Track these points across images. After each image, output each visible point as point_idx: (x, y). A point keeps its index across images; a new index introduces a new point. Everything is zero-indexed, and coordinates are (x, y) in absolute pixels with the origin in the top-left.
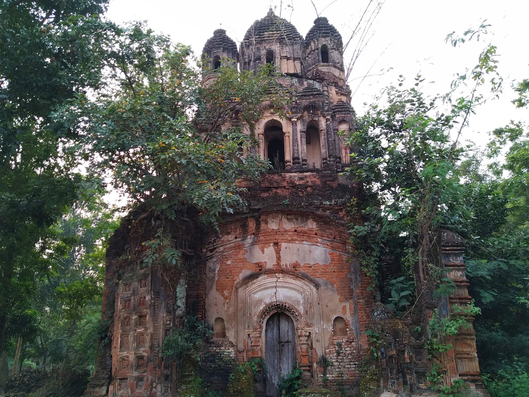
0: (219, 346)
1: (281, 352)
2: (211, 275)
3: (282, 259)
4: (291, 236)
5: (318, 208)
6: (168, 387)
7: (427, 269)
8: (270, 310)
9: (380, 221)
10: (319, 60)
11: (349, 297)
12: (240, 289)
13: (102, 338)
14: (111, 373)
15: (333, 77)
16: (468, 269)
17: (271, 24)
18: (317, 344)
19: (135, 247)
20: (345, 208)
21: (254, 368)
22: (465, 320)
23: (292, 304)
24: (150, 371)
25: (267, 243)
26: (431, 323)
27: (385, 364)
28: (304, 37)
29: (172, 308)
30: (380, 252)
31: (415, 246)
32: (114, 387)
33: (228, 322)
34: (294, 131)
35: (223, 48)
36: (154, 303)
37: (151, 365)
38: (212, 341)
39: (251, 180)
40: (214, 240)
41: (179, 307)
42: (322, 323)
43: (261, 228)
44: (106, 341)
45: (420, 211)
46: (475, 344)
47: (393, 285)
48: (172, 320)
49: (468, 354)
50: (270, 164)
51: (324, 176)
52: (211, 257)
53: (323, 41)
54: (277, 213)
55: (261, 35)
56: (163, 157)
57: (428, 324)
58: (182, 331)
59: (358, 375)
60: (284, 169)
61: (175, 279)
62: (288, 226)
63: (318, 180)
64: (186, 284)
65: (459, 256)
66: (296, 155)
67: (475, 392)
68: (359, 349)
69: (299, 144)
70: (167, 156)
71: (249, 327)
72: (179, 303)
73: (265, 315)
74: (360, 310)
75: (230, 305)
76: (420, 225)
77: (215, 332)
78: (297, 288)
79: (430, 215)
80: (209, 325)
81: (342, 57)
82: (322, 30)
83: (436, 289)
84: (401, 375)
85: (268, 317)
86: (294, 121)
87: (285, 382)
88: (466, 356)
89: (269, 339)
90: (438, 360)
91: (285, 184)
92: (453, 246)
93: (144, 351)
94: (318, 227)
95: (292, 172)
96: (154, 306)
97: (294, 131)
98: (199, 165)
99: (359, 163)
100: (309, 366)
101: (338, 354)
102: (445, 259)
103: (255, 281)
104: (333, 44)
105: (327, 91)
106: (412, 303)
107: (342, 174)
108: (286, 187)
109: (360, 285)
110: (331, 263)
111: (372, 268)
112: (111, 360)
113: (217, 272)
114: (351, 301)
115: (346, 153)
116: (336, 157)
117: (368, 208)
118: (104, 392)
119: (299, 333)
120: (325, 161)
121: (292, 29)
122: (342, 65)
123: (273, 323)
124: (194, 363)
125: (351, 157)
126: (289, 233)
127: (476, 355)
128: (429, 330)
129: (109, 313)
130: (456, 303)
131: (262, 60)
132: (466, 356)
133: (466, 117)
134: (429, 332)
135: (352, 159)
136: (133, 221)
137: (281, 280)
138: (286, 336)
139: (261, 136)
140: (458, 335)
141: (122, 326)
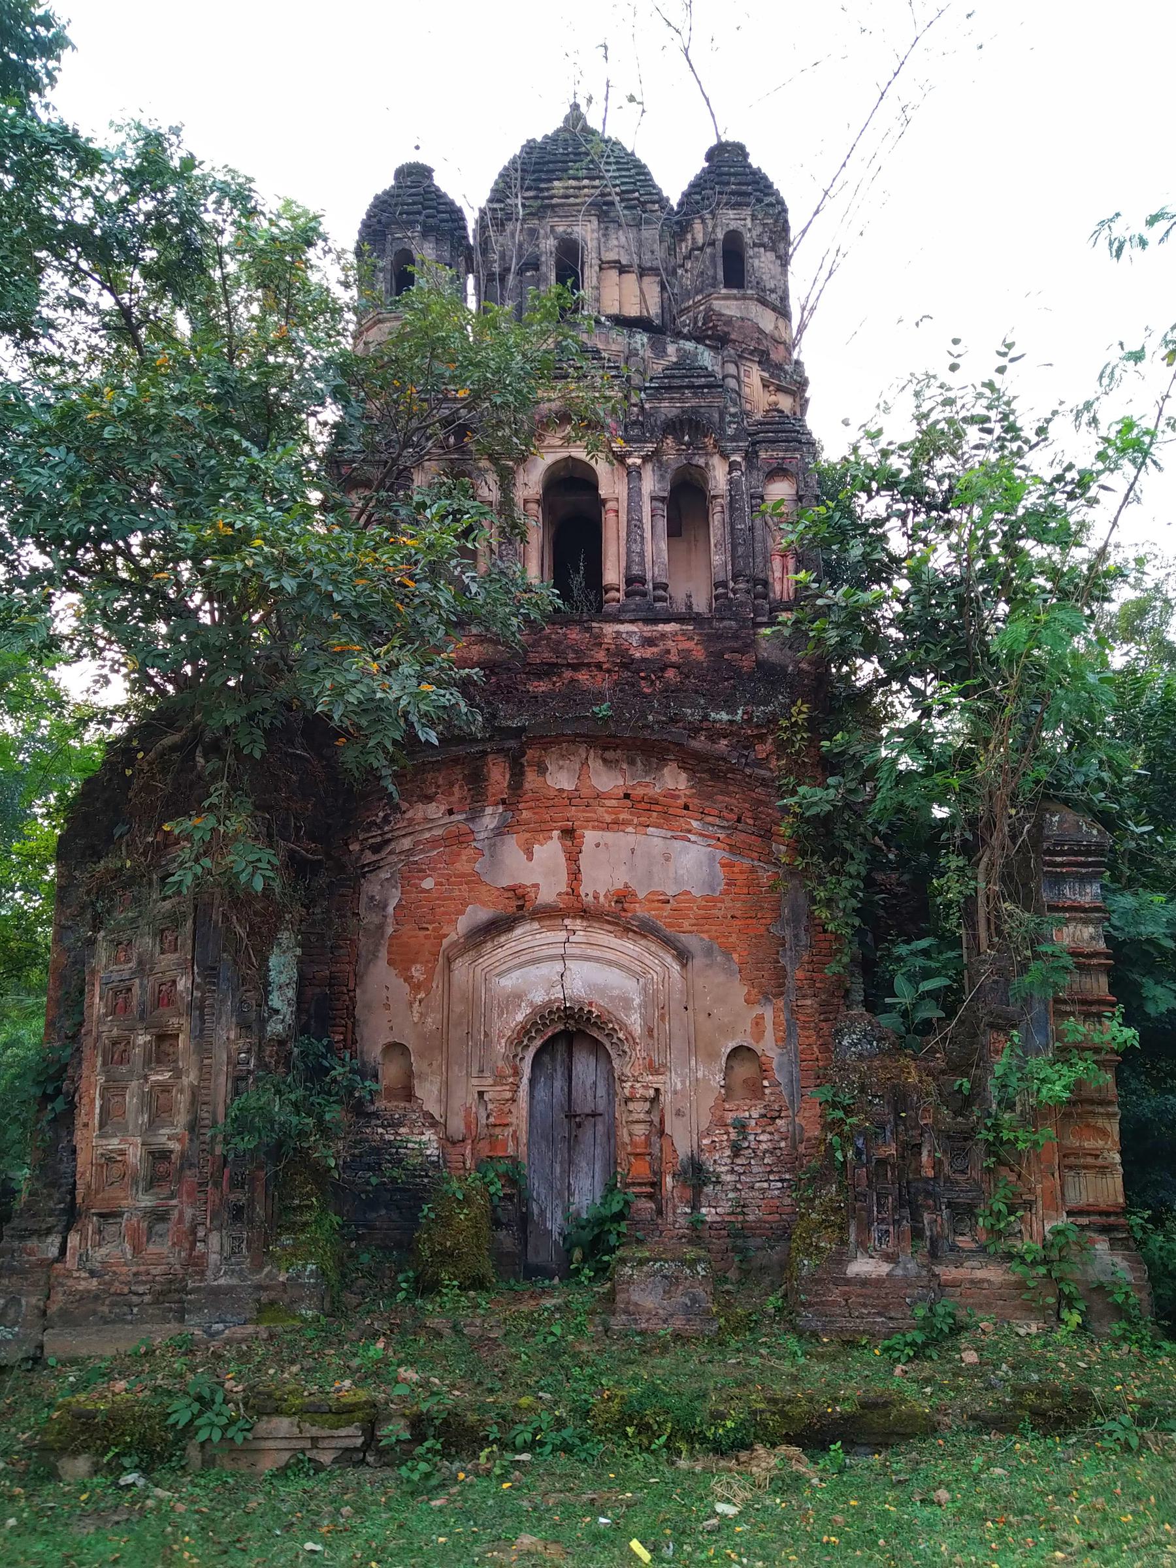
0: (395, 1125)
1: (572, 1142)
2: (370, 919)
3: (584, 877)
4: (614, 810)
5: (695, 731)
6: (241, 1241)
7: (998, 917)
8: (544, 1024)
10: (715, 278)
12: (458, 963)
13: (47, 1098)
14: (74, 1198)
17: (576, 154)
18: (678, 1122)
19: (147, 834)
20: (772, 732)
21: (492, 1189)
22: (1095, 1062)
23: (610, 1007)
24: (189, 1195)
25: (541, 830)
26: (999, 1070)
27: (864, 1182)
28: (674, 202)
29: (253, 1015)
31: (968, 850)
32: (84, 1238)
33: (421, 1056)
34: (634, 494)
35: (424, 225)
36: (203, 999)
38: (372, 1108)
40: (386, 817)
41: (277, 1012)
42: (693, 1062)
43: (527, 786)
44: (59, 1105)
45: (987, 751)
47: (900, 959)
49: (1097, 1156)
51: (718, 637)
52: (376, 867)
53: (730, 219)
54: (574, 742)
57: (992, 1072)
60: (599, 609)
61: (264, 930)
62: (606, 781)
65: (1091, 883)
66: (636, 570)
67: (1108, 1259)
69: (648, 535)
70: (239, 566)
72: (276, 1001)
73: (531, 1039)
74: (803, 1028)
78: (625, 960)
80: (364, 1064)
82: (728, 183)
84: (906, 1212)
85: (538, 1043)
88: (1090, 1160)
89: (540, 1107)
91: (601, 656)
92: (1076, 854)
93: (172, 1137)
94: (692, 787)
95: (622, 622)
96: (201, 1008)
97: (634, 494)
98: (335, 595)
99: (820, 602)
100: (653, 1185)
101: (736, 1151)
102: (1051, 889)
103: (503, 939)
104: (759, 229)
106: (951, 1013)
107: (768, 631)
109: (806, 958)
110: (726, 892)
112: (75, 1160)
113: (390, 910)
114: (780, 1003)
115: (784, 568)
116: (756, 581)
117: (839, 736)
118: (54, 1252)
120: (721, 590)
122: (784, 298)
123: (553, 1059)
124: (319, 1174)
126: (608, 803)
127: (1117, 1158)
131: (544, 269)
132: (1090, 1160)
134: (993, 1092)
136: (140, 755)
138: (590, 1098)
139: (533, 506)
141: (104, 1064)
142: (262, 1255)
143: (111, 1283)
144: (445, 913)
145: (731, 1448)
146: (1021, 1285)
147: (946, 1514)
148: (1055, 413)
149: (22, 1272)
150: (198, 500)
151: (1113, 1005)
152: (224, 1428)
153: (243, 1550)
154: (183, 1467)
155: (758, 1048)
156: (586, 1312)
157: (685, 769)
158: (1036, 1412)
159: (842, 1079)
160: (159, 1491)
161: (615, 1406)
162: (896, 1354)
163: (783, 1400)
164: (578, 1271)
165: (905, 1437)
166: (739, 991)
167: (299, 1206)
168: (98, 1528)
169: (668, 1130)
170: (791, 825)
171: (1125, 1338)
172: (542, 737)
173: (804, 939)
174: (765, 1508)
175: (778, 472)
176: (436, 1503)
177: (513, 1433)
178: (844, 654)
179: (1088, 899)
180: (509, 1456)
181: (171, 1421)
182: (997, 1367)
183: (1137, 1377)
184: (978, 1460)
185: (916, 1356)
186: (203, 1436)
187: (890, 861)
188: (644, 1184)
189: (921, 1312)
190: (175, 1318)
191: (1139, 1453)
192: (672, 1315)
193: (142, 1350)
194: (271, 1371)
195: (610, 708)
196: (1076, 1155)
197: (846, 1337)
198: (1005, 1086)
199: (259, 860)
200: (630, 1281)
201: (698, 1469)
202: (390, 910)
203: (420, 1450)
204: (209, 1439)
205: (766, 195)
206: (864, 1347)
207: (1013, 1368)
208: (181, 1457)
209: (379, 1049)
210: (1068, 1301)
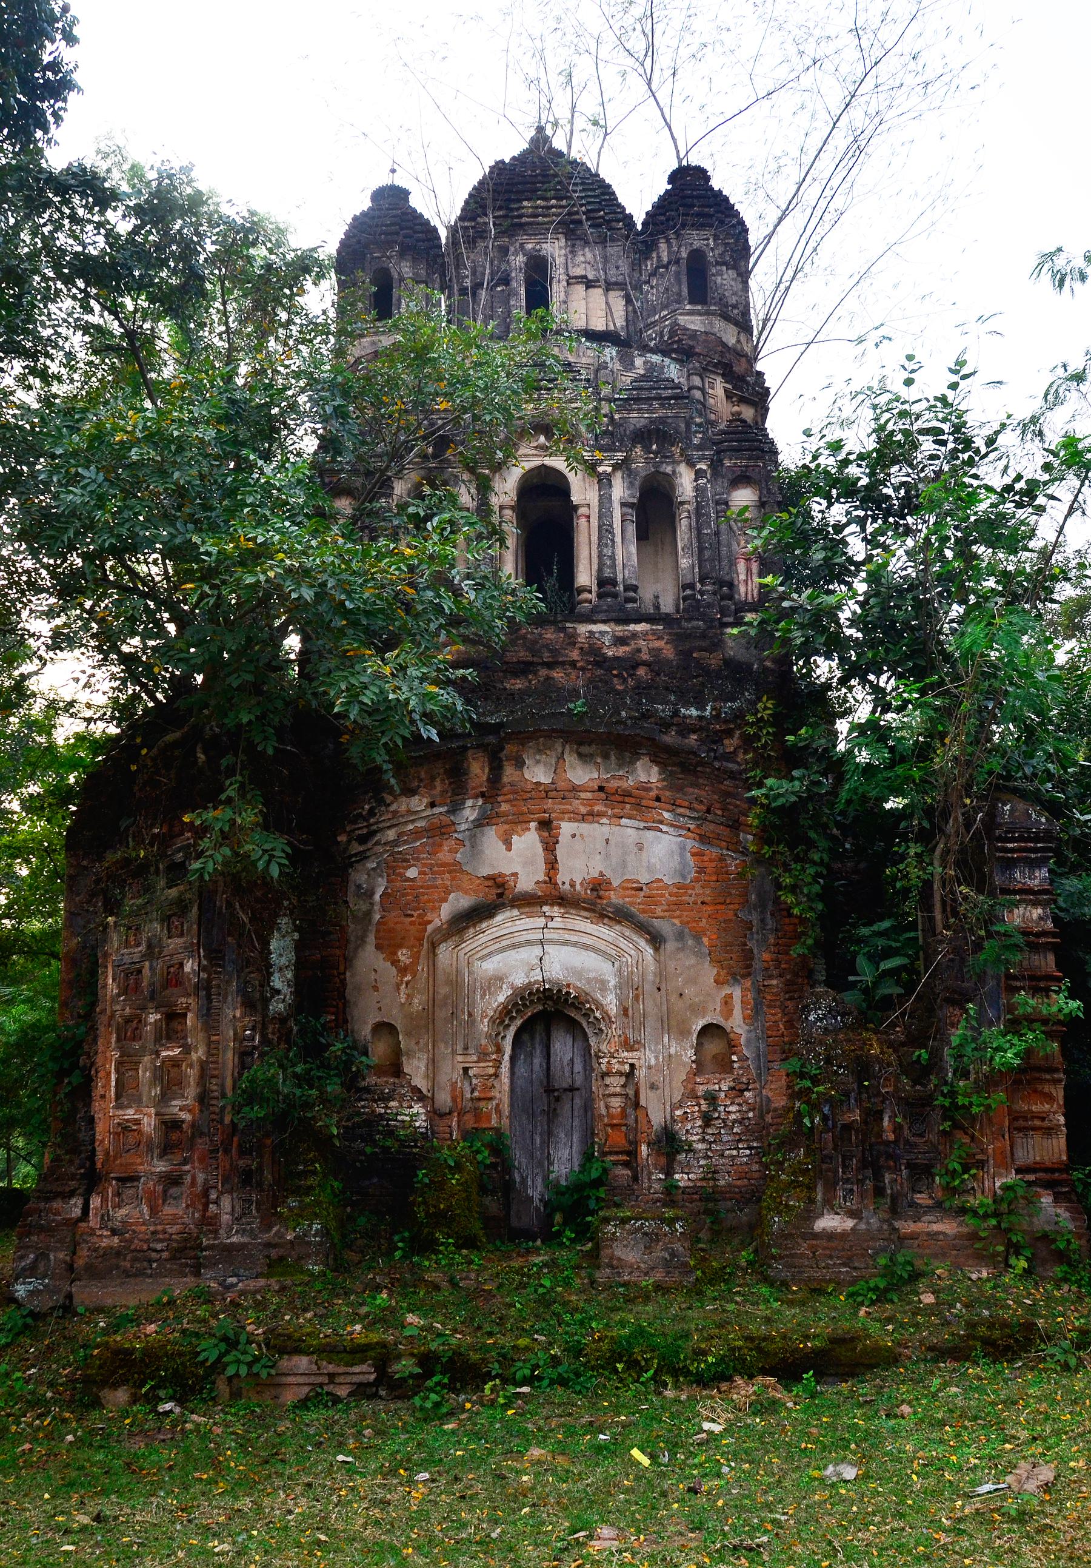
0: (386, 1099)
1: (551, 1115)
3: (560, 866)
5: (665, 725)
6: (250, 1202)
7: (955, 900)
8: (524, 1005)
9: (838, 766)
10: (679, 294)
11: (743, 971)
12: (443, 947)
13: (61, 1074)
14: (93, 1163)
15: (720, 349)
16: (1060, 900)
17: (544, 176)
18: (651, 1094)
19: (152, 826)
20: (740, 727)
21: (480, 1157)
22: (1043, 1032)
23: (586, 988)
24: (201, 1160)
25: (519, 822)
26: (955, 1041)
27: (830, 1145)
28: (639, 219)
29: (257, 995)
30: (831, 851)
31: (926, 837)
32: (104, 1200)
33: (408, 1034)
34: (605, 501)
35: (401, 245)
36: (209, 981)
37: (202, 1144)
38: (364, 1084)
39: (481, 643)
41: (278, 992)
42: (666, 1039)
43: (505, 779)
44: (76, 1079)
45: (944, 745)
46: (1061, 1093)
47: (860, 941)
48: (259, 1026)
49: (1043, 1119)
50: (538, 598)
52: (363, 857)
53: (698, 239)
54: (550, 737)
55: (512, 210)
56: (250, 580)
57: (949, 1043)
58: (287, 1058)
59: (756, 1175)
60: (572, 610)
61: (266, 914)
62: (581, 774)
63: (669, 646)
64: (297, 929)
66: (607, 573)
67: (1051, 1211)
68: (762, 1108)
69: (618, 539)
70: (262, 578)
71: (466, 1048)
72: (277, 982)
73: (512, 1019)
74: (769, 1006)
75: (413, 988)
76: (942, 781)
77: (374, 1060)
78: (602, 945)
79: (972, 754)
80: (355, 1041)
81: (746, 288)
83: (975, 952)
84: (869, 1172)
85: (519, 1022)
86: (604, 472)
87: (563, 1194)
88: (1037, 1123)
89: (520, 1082)
90: (966, 1133)
91: (575, 655)
93: (182, 1109)
94: (663, 780)
95: (595, 622)
96: (208, 988)
97: (605, 501)
98: (347, 603)
99: (785, 604)
100: (628, 1153)
101: (707, 1120)
102: (1003, 873)
103: (484, 925)
104: (721, 249)
105: (702, 390)
106: (910, 987)
107: (735, 631)
108: (579, 665)
110: (696, 880)
111: (807, 895)
112: (93, 1129)
113: (377, 897)
114: (748, 983)
115: (749, 570)
116: (721, 583)
117: (803, 731)
118: (77, 1212)
119: (603, 1067)
120: (688, 592)
121: (603, 194)
122: (746, 313)
123: (532, 1038)
124: (322, 1141)
125: (762, 586)
126: (583, 795)
127: (1062, 1120)
128: (948, 1059)
129: (80, 1006)
130: (1023, 988)
131: (514, 284)
132: (1037, 1123)
133: (1079, 491)
134: (949, 1062)
135: (765, 591)
136: (144, 752)
137: (558, 923)
139: (508, 512)
140: (1020, 1070)
141: (118, 1040)
142: (269, 1218)
143: (131, 1241)
144: (429, 901)
145: (712, 1380)
146: (974, 1236)
147: (909, 1424)
148: (1003, 426)
149: (48, 1230)
150: (214, 514)
151: (1059, 980)
152: (250, 1365)
153: (282, 1461)
154: (213, 1399)
155: (727, 1026)
156: (573, 1268)
157: (657, 763)
158: (987, 1342)
159: (809, 1052)
160: (195, 1417)
161: (605, 1346)
162: (860, 1299)
163: (758, 1338)
164: (559, 1234)
165: (871, 1367)
166: (709, 973)
167: (303, 1171)
168: (147, 1445)
169: (642, 1102)
170: (758, 816)
171: (1065, 1280)
172: (520, 732)
173: (770, 923)
174: (748, 1426)
175: (740, 480)
176: (448, 1427)
177: (513, 1370)
178: (807, 651)
179: (1037, 882)
180: (513, 1390)
181: (201, 1358)
182: (952, 1306)
183: (1077, 1310)
184: (936, 1382)
185: (878, 1300)
186: (231, 1371)
187: (845, 850)
188: (621, 1153)
189: (882, 1261)
190: (192, 1273)
191: (1077, 1371)
192: (652, 1269)
193: (165, 1300)
194: (287, 1317)
195: (584, 704)
196: (1026, 1119)
197: (815, 1285)
198: (961, 1056)
199: (273, 849)
200: (613, 1238)
201: (683, 1397)
202: (377, 897)
203: (430, 1383)
204: (237, 1375)
205: (727, 216)
206: (830, 1294)
207: (966, 1306)
208: (211, 1390)
209: (369, 1027)
210: (1016, 1249)
